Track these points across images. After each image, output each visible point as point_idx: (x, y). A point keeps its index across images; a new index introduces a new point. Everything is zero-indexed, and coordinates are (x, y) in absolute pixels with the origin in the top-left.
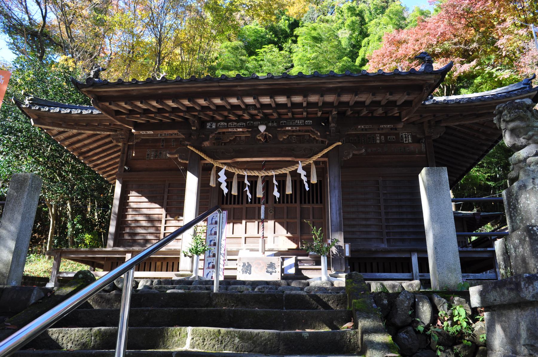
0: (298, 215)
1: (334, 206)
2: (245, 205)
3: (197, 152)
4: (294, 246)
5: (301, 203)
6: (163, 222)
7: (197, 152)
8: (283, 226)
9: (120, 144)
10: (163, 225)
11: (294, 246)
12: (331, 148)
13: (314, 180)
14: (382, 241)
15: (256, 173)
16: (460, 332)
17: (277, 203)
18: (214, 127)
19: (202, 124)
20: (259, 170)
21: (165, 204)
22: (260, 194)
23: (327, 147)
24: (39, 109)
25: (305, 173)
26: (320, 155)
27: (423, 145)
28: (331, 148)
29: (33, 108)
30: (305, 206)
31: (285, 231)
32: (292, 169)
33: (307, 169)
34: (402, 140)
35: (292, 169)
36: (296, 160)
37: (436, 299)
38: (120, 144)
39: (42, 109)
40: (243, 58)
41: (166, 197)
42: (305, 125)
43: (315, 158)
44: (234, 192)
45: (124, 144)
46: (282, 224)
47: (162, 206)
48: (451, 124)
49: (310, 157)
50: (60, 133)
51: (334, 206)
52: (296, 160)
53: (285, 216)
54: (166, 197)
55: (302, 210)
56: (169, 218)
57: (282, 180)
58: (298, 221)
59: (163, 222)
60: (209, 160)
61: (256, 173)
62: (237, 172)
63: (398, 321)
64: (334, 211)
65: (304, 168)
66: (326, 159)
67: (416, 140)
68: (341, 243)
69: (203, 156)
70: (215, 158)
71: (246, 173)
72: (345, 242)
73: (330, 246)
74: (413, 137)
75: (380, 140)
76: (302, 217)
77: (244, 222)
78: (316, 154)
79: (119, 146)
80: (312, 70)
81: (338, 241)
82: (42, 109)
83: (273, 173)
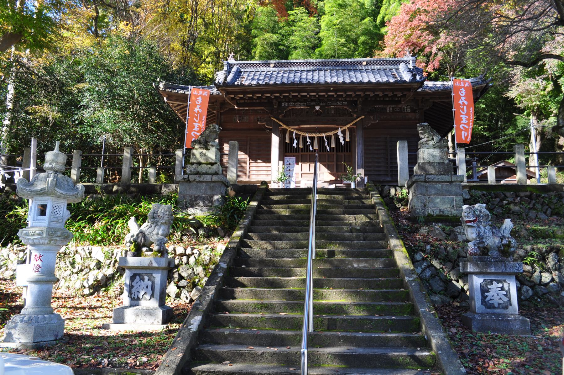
0: (335, 160)
1: (359, 154)
2: (308, 153)
3: (277, 121)
4: (333, 178)
5: (337, 152)
6: (248, 163)
7: (277, 121)
8: (325, 167)
9: (215, 112)
10: (248, 166)
11: (333, 178)
12: (358, 120)
13: (348, 139)
14: (387, 176)
15: (313, 135)
16: (403, 197)
17: (300, 150)
18: (286, 105)
19: (280, 104)
20: (314, 132)
21: (248, 152)
22: (316, 147)
23: (356, 119)
24: (171, 91)
25: (342, 135)
26: (351, 124)
27: (417, 114)
28: (358, 120)
29: (167, 90)
30: (339, 154)
31: (327, 170)
32: (335, 132)
33: (344, 132)
34: (404, 110)
35: (335, 132)
36: (337, 127)
37: (397, 188)
38: (215, 112)
39: (173, 91)
40: (276, 18)
41: (248, 148)
42: (343, 105)
43: (348, 126)
44: (301, 146)
45: (218, 111)
46: (325, 165)
47: (246, 153)
48: (436, 101)
49: (346, 125)
50: (179, 105)
51: (359, 154)
52: (337, 127)
53: (327, 160)
54: (248, 148)
55: (337, 156)
56: (251, 161)
57: (329, 138)
58: (335, 163)
59: (248, 163)
60: (284, 126)
61: (313, 135)
62: (302, 134)
63: (384, 195)
64: (359, 157)
65: (342, 132)
66: (355, 126)
67: (413, 111)
68: (363, 175)
69: (281, 124)
70: (288, 125)
71: (307, 135)
72: (365, 175)
73: (355, 177)
74: (411, 108)
75: (390, 110)
76: (337, 161)
77: (300, 163)
78: (349, 123)
79: (214, 113)
80: (332, 7)
81: (360, 174)
82: (173, 91)
83: (324, 135)
